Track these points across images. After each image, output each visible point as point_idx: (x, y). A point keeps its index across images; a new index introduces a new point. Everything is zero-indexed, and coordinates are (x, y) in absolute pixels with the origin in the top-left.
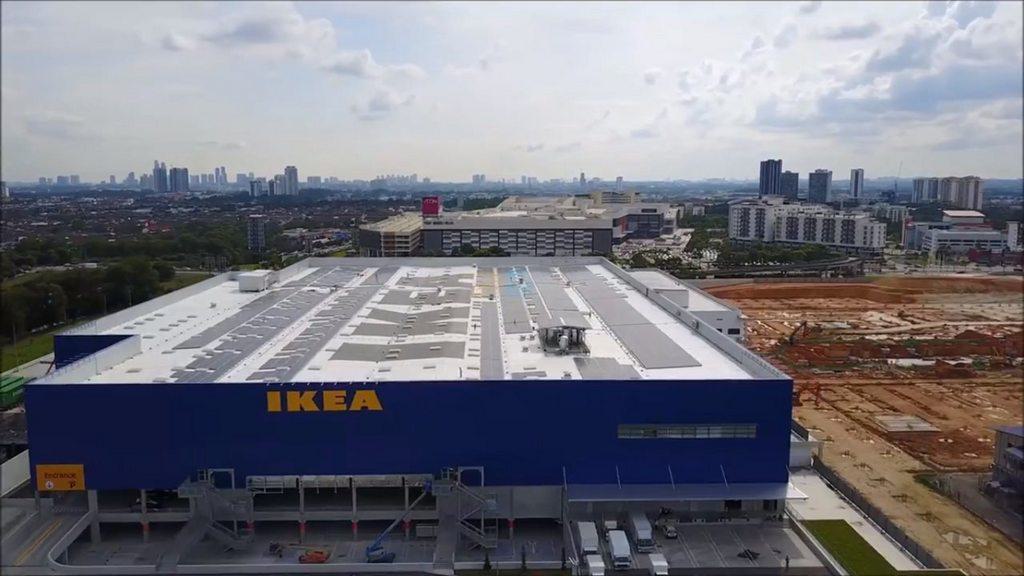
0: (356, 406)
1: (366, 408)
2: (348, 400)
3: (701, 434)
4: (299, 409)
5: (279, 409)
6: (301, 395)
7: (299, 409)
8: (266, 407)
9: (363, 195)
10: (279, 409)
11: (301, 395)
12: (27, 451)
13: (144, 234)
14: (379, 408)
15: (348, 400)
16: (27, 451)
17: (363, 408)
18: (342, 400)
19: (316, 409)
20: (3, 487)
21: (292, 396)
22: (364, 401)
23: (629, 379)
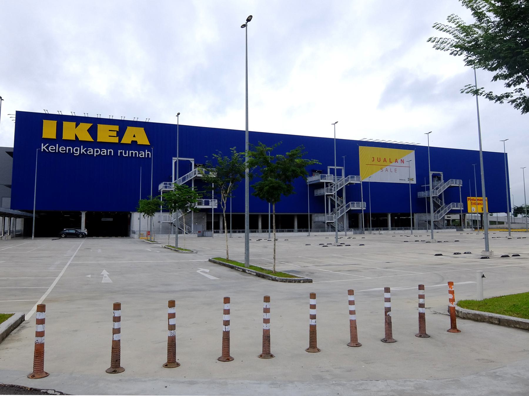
0: (127, 139)
1: (136, 142)
2: (120, 134)
3: (460, 190)
4: (74, 139)
5: (6, 218)
6: (77, 126)
7: (74, 139)
8: (62, 138)
9: (449, 228)
10: (6, 218)
11: (77, 126)
12: (121, 142)
13: (213, 159)
14: (150, 144)
15: (120, 134)
16: (121, 142)
17: (132, 141)
18: (115, 134)
19: (91, 140)
20: (91, 125)
21: (66, 125)
22: (134, 136)
23: (108, 117)
